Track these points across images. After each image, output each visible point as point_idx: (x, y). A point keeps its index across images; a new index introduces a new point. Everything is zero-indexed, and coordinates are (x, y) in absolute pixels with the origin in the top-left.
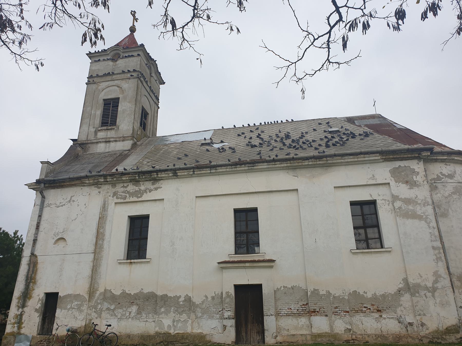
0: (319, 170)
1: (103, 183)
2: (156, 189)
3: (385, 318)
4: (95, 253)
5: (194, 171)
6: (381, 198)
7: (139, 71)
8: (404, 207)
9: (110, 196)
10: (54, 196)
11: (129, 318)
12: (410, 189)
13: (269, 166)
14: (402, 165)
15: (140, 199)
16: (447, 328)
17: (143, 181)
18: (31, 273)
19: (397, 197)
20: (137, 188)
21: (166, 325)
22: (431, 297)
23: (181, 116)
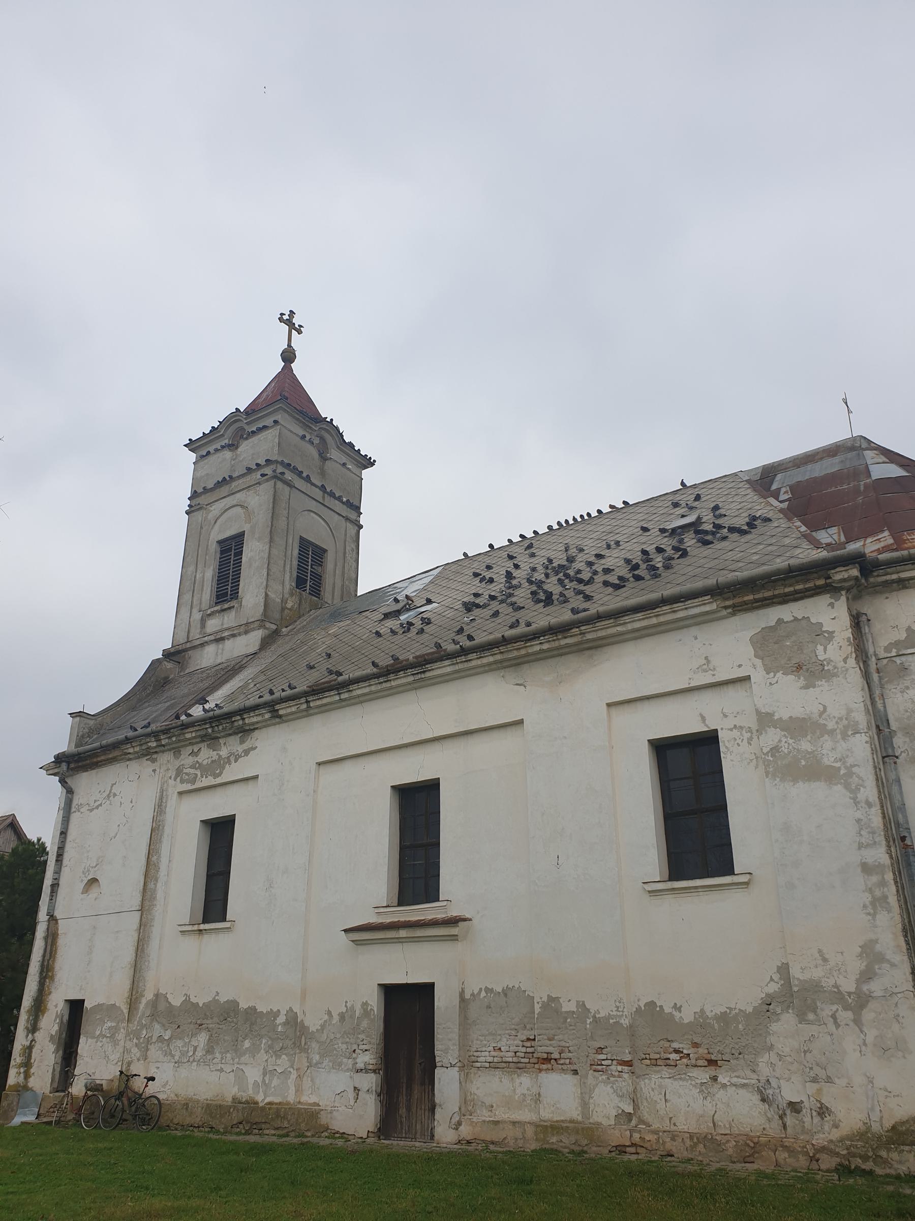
0: (573, 661)
1: (157, 750)
2: (247, 752)
3: (724, 1086)
4: (141, 910)
5: (307, 702)
6: (730, 723)
7: (276, 462)
8: (787, 744)
9: (170, 778)
10: (88, 784)
11: (194, 1061)
12: (806, 687)
13: (457, 667)
14: (787, 617)
15: (219, 780)
16: (894, 1128)
17: (223, 737)
18: (47, 957)
19: (770, 715)
20: (214, 754)
21: (251, 1081)
22: (851, 1024)
23: (407, 536)
